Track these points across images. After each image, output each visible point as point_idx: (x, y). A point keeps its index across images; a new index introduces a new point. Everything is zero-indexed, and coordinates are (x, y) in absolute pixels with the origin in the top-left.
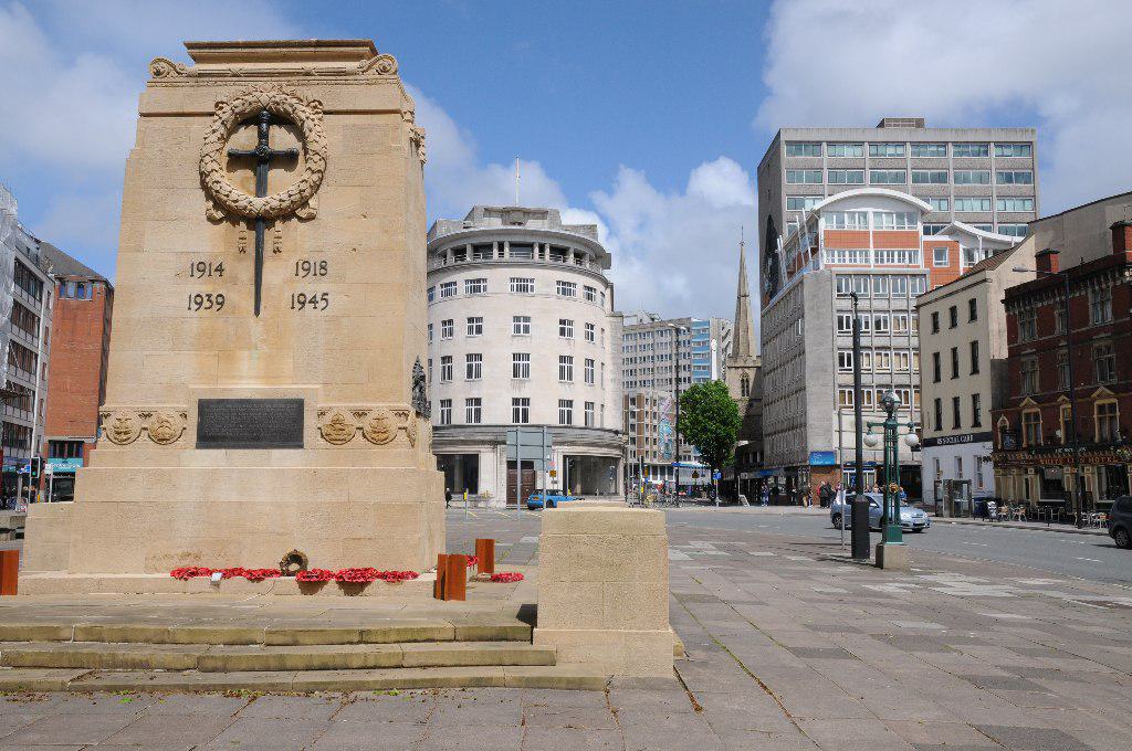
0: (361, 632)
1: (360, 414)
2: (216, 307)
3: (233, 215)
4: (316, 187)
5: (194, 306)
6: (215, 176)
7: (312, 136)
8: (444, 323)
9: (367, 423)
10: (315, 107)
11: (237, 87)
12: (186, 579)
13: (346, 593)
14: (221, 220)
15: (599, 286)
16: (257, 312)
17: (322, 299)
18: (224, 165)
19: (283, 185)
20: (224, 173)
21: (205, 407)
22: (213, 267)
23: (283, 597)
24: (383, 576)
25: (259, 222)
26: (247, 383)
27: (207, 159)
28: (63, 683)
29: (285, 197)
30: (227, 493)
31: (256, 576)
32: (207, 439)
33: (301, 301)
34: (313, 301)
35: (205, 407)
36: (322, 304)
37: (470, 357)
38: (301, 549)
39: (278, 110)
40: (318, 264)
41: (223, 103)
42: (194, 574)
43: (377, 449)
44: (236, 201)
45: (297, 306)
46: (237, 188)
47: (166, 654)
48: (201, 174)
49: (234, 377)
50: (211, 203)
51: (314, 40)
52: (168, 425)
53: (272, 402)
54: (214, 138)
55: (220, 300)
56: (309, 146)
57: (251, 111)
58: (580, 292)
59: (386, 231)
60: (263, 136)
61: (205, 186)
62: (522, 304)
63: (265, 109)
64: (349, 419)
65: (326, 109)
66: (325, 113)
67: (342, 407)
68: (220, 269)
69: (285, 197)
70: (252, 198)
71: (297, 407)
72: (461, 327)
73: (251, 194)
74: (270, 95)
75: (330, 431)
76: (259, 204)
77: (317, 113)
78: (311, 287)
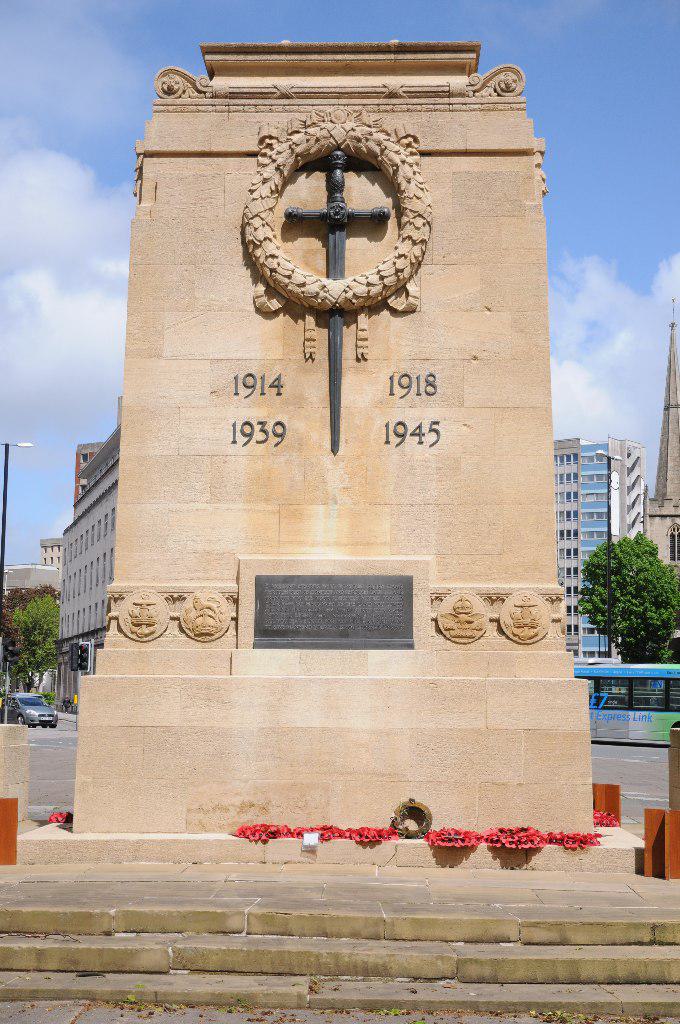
0: (654, 927)
1: (494, 599)
2: (274, 440)
3: (296, 306)
4: (417, 265)
5: (241, 439)
6: (270, 248)
7: (411, 190)
9: (505, 612)
10: (409, 145)
11: (291, 115)
12: (265, 842)
13: (504, 865)
14: (276, 313)
16: (335, 448)
17: (431, 430)
18: (278, 232)
19: (367, 262)
20: (278, 242)
21: (265, 587)
22: (269, 381)
23: (407, 865)
24: (552, 839)
25: (334, 315)
26: (323, 551)
27: (257, 222)
28: (300, 996)
29: (374, 279)
30: (305, 714)
31: (368, 838)
32: (269, 633)
33: (400, 431)
34: (418, 433)
35: (265, 587)
38: (422, 799)
39: (358, 149)
40: (422, 380)
41: (271, 137)
42: (275, 834)
43: (521, 651)
44: (303, 285)
45: (395, 440)
46: (299, 263)
47: (411, 956)
48: (245, 243)
49: (301, 543)
50: (261, 288)
51: (396, 41)
52: (211, 613)
53: (365, 579)
54: (265, 190)
55: (279, 430)
56: (407, 204)
57: (319, 150)
59: (522, 331)
60: (334, 189)
61: (251, 262)
63: (339, 149)
64: (479, 606)
65: (423, 147)
66: (423, 154)
67: (465, 588)
68: (277, 385)
70: (325, 281)
71: (403, 588)
73: (318, 272)
74: (349, 125)
75: (449, 623)
76: (335, 290)
77: (412, 154)
78: (416, 413)
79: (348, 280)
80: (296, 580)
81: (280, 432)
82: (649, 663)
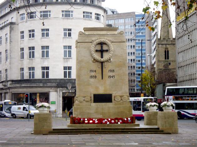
2: (95, 78)
8: (30, 31)
15: (101, 12)
16: (102, 79)
19: (106, 56)
21: (95, 95)
25: (102, 63)
34: (112, 77)
35: (95, 95)
36: (113, 77)
37: (43, 47)
45: (109, 78)
46: (97, 56)
58: (93, 16)
62: (68, 23)
69: (107, 58)
70: (101, 59)
72: (38, 34)
76: (102, 60)
79: (103, 59)
80: (32, 81)
81: (96, 77)
82: (187, 116)
